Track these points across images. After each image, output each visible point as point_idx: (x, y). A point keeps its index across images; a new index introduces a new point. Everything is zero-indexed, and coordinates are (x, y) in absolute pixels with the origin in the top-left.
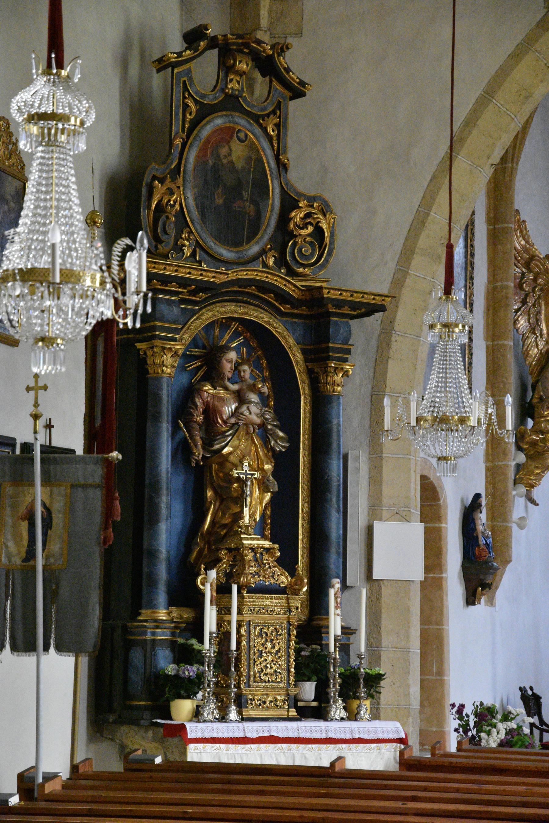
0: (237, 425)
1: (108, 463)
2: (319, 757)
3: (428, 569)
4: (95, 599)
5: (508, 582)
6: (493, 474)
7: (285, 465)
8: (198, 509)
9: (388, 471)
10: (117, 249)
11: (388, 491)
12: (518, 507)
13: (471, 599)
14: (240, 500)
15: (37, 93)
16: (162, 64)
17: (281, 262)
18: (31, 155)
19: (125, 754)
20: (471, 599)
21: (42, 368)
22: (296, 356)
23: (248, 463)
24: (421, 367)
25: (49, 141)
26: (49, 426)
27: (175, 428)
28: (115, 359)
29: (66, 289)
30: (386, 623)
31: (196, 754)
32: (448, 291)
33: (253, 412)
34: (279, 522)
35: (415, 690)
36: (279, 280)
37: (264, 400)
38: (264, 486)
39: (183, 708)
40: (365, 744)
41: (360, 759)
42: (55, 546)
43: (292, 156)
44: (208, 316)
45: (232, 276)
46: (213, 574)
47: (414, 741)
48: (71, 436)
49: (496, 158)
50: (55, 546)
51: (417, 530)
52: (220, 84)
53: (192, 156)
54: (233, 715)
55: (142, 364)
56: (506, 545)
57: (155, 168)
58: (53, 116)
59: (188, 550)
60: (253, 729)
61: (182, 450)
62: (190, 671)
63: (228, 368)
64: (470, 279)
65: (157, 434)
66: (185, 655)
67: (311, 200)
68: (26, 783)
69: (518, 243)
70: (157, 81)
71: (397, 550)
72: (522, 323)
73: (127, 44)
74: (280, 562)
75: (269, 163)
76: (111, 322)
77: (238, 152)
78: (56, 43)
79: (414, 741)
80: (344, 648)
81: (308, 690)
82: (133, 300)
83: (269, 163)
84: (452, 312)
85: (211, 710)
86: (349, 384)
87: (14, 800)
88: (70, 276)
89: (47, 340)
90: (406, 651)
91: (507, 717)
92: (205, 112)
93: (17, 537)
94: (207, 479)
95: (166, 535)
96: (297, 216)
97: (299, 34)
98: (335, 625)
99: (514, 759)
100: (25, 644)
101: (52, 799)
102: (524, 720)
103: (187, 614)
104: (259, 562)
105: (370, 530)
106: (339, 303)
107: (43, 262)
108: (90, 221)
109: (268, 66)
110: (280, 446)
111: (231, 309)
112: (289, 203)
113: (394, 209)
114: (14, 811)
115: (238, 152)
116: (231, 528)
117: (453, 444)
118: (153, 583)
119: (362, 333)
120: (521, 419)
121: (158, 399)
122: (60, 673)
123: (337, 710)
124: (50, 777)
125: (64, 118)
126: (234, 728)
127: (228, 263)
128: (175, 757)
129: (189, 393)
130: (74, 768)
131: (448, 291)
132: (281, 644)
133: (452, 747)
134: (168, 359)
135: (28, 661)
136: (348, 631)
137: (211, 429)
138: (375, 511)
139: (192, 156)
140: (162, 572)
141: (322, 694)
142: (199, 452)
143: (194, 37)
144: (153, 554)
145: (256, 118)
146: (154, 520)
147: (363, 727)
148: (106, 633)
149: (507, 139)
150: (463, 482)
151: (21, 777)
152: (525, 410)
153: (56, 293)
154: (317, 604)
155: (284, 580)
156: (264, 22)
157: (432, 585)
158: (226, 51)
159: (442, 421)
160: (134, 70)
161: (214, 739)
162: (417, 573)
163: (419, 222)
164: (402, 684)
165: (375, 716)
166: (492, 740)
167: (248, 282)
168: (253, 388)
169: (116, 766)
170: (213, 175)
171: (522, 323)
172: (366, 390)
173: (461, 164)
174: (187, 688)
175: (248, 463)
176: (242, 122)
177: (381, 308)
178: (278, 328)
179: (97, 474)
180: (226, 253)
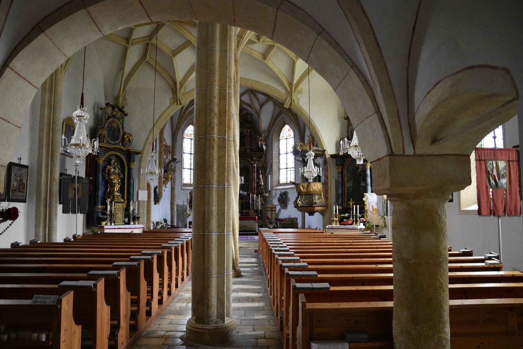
0: (114, 173)
1: (90, 180)
2: (129, 231)
3: (148, 199)
4: (87, 204)
5: (162, 201)
6: (160, 182)
7: (123, 180)
8: (106, 188)
9: (141, 182)
10: (93, 141)
11: (141, 185)
12: (164, 188)
13: (155, 204)
14: (114, 186)
15: (78, 112)
16: (101, 109)
17: (122, 144)
18: (76, 123)
19: (93, 232)
20: (155, 204)
21: (78, 162)
22: (125, 161)
23: (116, 181)
24: (147, 163)
25: (80, 121)
26: (78, 173)
27: (102, 174)
28: (91, 160)
29: (83, 148)
30: (140, 208)
31: (106, 231)
32: (153, 151)
33: (117, 171)
34: (121, 191)
35: (146, 219)
36: (122, 148)
37: (119, 169)
38: (119, 184)
39: (104, 223)
40: (137, 229)
41: (136, 231)
42: (80, 195)
43: (125, 126)
44: (107, 155)
45: (113, 146)
46: (109, 200)
47: (145, 228)
48: (83, 174)
49: (161, 128)
50: (80, 195)
51: (146, 192)
52: (112, 113)
53: (106, 125)
54: (113, 224)
55: (96, 162)
56: (162, 195)
57: (99, 127)
58: (81, 116)
59: (105, 195)
60: (118, 227)
61: (104, 178)
62: (105, 217)
63: (112, 163)
64: (156, 149)
65: (99, 174)
66: (104, 214)
67: (128, 134)
68: (74, 237)
69: (164, 143)
70: (100, 112)
71: (143, 195)
72: (165, 157)
73: (95, 104)
74: (122, 197)
75: (121, 127)
76: (91, 154)
77: (115, 125)
78: (82, 103)
79: (145, 228)
80: (133, 212)
81: (127, 220)
82: (95, 150)
83: (121, 127)
84: (153, 154)
85: (109, 224)
86: (134, 166)
87: (72, 240)
88: (84, 145)
89: (79, 157)
90: (144, 213)
91: (161, 223)
92: (109, 117)
93: (72, 193)
94: (108, 183)
95: (100, 193)
96: (126, 136)
97: (127, 105)
98: (132, 208)
99: (163, 230)
100: (74, 212)
101: (79, 239)
102: (164, 224)
103: (104, 207)
104: (118, 197)
105: (138, 192)
106: (133, 152)
107: (79, 142)
108: (87, 136)
109: (121, 110)
110: (122, 177)
111: (113, 153)
112: (124, 134)
113: (143, 136)
114: (72, 242)
115: (115, 125)
116: (112, 191)
117: (153, 177)
118: (98, 201)
119: (137, 157)
120: (164, 173)
121: (99, 168)
122: (80, 217)
123: (132, 223)
124: (79, 236)
125: (83, 117)
126: (113, 226)
127: (113, 144)
128: (102, 232)
129: (105, 167)
130: (83, 234)
131: (153, 151)
132: (122, 212)
133: (152, 229)
134: (101, 161)
135: (75, 215)
136: (134, 209)
137: (109, 174)
138: (139, 188)
139: (106, 125)
140: (100, 199)
141: (129, 221)
142: (107, 178)
143: (107, 104)
144: (98, 196)
145: (118, 119)
146: (98, 190)
147: (137, 226)
148: (89, 210)
149: (163, 125)
150: (154, 184)
151: (73, 236)
152: (165, 172)
153: (81, 148)
154: (128, 205)
155: (122, 201)
156: (120, 102)
157: (149, 202)
158: (113, 107)
159: (151, 173)
160: (96, 110)
161: (109, 228)
162: (146, 200)
163: (148, 138)
164: (143, 218)
165: (138, 224)
166: (159, 227)
167: (116, 148)
168: (117, 167)
169: (91, 233)
170: (110, 129)
171: (165, 157)
172: (138, 167)
173: (155, 129)
174: (105, 220)
175: (116, 181)
176: (116, 120)
177: (140, 153)
178: (122, 156)
179: (88, 182)
180: (112, 142)
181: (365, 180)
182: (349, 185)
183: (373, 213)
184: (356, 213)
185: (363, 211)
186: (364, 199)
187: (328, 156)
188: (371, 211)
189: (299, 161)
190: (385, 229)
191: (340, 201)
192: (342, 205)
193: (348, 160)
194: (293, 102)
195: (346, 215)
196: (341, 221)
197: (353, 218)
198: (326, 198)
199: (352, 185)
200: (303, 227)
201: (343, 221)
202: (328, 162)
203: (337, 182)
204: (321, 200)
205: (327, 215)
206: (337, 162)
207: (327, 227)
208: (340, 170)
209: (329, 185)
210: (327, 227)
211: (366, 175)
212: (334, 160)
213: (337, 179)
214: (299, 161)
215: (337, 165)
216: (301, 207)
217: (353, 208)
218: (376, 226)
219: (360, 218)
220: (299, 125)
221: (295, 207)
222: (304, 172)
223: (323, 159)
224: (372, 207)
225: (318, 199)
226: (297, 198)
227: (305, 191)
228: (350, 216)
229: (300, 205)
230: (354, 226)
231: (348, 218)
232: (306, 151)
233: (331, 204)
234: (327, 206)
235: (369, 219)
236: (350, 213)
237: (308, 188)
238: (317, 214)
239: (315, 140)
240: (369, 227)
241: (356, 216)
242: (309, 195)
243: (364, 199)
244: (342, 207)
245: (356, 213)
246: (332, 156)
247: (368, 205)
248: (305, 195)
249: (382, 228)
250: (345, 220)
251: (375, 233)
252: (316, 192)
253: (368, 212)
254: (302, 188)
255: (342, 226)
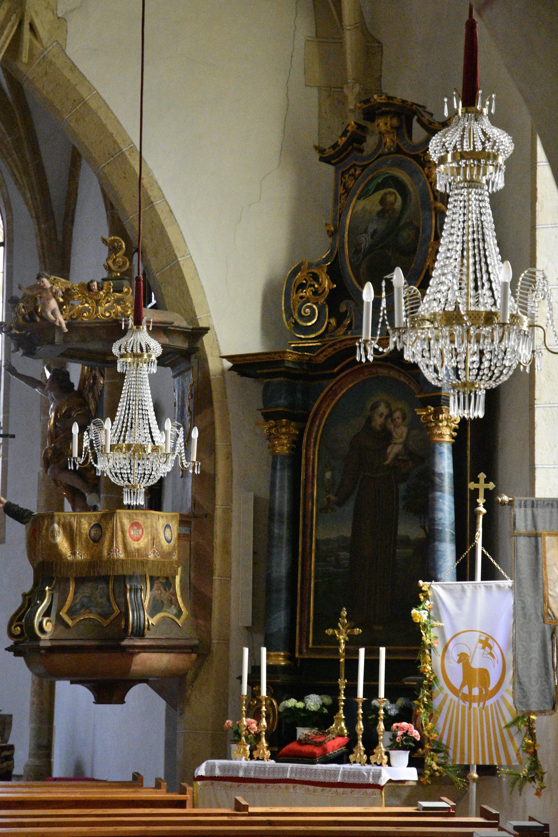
181: (425, 509)
182: (331, 529)
183: (468, 698)
184: (371, 690)
185: (410, 681)
186: (420, 615)
187: (216, 365)
188: (457, 679)
189: (33, 382)
190: (530, 789)
191: (280, 620)
192: (290, 648)
193: (333, 392)
194: (27, 35)
195: (313, 702)
196: (281, 740)
197: (351, 722)
198: (200, 603)
199: (347, 533)
200: (42, 772)
201: (292, 736)
202: (216, 396)
203: (264, 515)
204: (169, 613)
205: (201, 702)
206: (267, 399)
207: (201, 771)
208: (283, 447)
209: (218, 528)
210: (201, 771)
211: (428, 480)
212: (254, 388)
213: (265, 494)
214: (33, 382)
215: (267, 416)
216: (51, 650)
217: (353, 664)
218: (481, 769)
219: (389, 721)
220: (40, 170)
221: (16, 650)
222: (95, 451)
223: (190, 378)
224: (463, 658)
225: (155, 608)
226: (30, 600)
227: (81, 556)
228: (333, 708)
229: (45, 640)
230: (357, 767)
231: (322, 720)
232: (115, 330)
233: (226, 641)
234: (199, 650)
235: (441, 727)
236: (334, 692)
237: (97, 540)
238: (139, 694)
239: (145, 269)
240: (439, 776)
241: (371, 711)
242: (106, 578)
243: (420, 615)
244: (290, 657)
245: (371, 690)
246: (243, 365)
247: (438, 646)
248: (80, 581)
249: (519, 782)
250: (302, 732)
251: (484, 813)
252: (144, 563)
253: (442, 693)
254: (62, 542)
255: (290, 769)
